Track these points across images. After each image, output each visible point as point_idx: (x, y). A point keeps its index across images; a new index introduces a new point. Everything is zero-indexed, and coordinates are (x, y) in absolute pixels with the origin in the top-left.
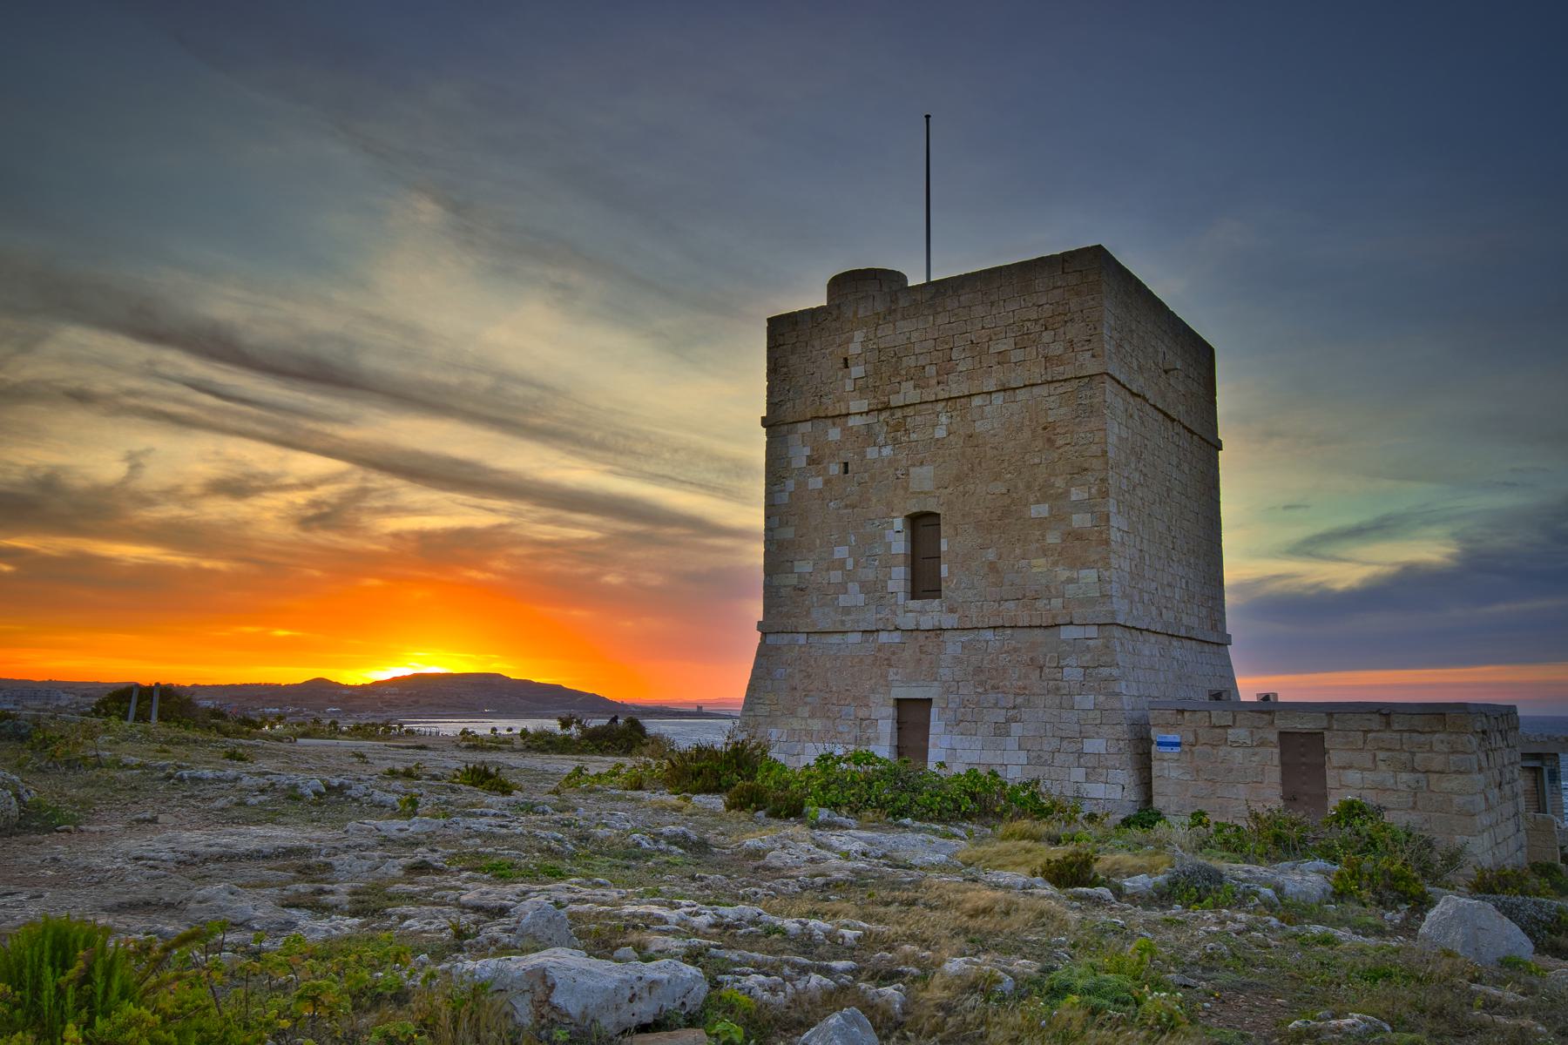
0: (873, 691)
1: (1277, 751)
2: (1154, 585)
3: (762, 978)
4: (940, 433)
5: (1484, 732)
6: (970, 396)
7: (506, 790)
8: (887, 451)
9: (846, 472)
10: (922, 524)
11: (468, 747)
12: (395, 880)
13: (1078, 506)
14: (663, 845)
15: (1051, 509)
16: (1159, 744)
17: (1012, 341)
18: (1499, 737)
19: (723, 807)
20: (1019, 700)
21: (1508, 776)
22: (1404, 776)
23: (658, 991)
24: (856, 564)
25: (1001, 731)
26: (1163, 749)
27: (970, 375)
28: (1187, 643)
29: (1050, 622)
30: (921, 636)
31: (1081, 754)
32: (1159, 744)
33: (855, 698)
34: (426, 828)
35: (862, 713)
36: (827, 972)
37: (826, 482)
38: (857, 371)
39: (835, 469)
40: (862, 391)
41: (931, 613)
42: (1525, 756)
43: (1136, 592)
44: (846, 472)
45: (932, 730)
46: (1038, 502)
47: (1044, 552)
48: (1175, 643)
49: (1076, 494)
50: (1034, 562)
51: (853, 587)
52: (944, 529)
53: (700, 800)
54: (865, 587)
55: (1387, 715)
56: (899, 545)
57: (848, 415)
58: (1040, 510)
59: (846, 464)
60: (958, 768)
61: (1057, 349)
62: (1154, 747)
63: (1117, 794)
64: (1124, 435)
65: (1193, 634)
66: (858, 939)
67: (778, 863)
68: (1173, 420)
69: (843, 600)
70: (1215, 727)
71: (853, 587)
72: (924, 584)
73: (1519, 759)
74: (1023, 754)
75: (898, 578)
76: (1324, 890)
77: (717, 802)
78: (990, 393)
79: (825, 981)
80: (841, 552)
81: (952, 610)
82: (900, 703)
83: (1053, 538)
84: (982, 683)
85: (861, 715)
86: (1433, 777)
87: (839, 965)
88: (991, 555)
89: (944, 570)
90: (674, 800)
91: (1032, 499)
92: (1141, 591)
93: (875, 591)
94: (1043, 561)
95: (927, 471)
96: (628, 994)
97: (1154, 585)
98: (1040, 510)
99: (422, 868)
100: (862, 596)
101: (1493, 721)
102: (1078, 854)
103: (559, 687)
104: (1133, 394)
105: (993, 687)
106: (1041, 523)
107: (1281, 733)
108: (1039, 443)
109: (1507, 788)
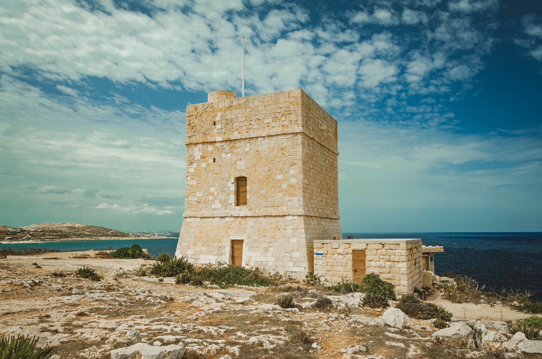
0: (223, 237)
1: (351, 256)
2: (316, 201)
3: (199, 347)
4: (247, 149)
5: (411, 249)
6: (257, 137)
7: (97, 278)
8: (229, 155)
9: (214, 162)
10: (241, 181)
11: (73, 257)
12: (74, 320)
13: (292, 176)
14: (159, 300)
15: (283, 176)
16: (316, 254)
17: (271, 119)
18: (415, 249)
19: (174, 283)
20: (272, 240)
21: (417, 261)
22: (388, 263)
23: (171, 354)
24: (218, 194)
25: (266, 250)
26: (317, 256)
27: (258, 129)
28: (326, 220)
29: (283, 215)
30: (240, 219)
31: (292, 257)
32: (316, 254)
33: (217, 240)
34: (77, 299)
35: (220, 245)
36: (217, 344)
37: (207, 165)
38: (218, 126)
39: (211, 161)
40: (219, 133)
41: (243, 210)
42: (423, 253)
43: (310, 204)
44: (214, 162)
45: (244, 250)
46: (279, 174)
47: (281, 191)
48: (322, 220)
49: (292, 172)
50: (278, 194)
51: (217, 201)
52: (248, 182)
53: (167, 280)
54: (221, 202)
55: (383, 245)
56: (233, 188)
57: (215, 142)
58: (280, 177)
59: (215, 159)
60: (252, 264)
61: (286, 123)
62: (315, 255)
63: (302, 270)
64: (307, 152)
65: (328, 216)
66: (225, 332)
67: (197, 305)
68: (323, 146)
69: (213, 206)
71: (217, 201)
72: (240, 199)
73: (421, 255)
74: (273, 258)
75: (232, 198)
76: (360, 303)
77: (172, 280)
78: (264, 137)
79: (217, 346)
80: (212, 189)
81: (251, 210)
82: (233, 241)
83: (284, 186)
84: (260, 235)
85: (219, 245)
86: (396, 263)
87: (220, 341)
88: (264, 191)
89: (248, 196)
90: (157, 280)
92: (312, 203)
93: (225, 204)
94: (280, 194)
95: (243, 162)
96: (163, 356)
97: (316, 201)
98: (280, 177)
99: (82, 314)
101: (414, 245)
104: (311, 139)
105: (264, 236)
106: (280, 181)
108: (280, 154)
109: (417, 265)
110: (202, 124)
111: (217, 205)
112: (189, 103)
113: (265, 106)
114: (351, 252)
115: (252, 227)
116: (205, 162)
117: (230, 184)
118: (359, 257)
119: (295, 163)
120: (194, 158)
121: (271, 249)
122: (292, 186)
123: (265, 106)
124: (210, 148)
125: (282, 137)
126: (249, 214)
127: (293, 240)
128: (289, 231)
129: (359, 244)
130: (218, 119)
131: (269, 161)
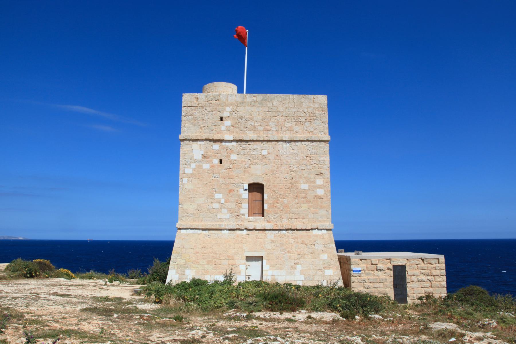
10: (256, 188)
15: (309, 186)
25: (293, 267)
37: (212, 167)
38: (227, 123)
39: (216, 162)
41: (259, 222)
46: (304, 183)
50: (302, 205)
54: (231, 211)
58: (304, 186)
70: (373, 264)
71: (224, 211)
91: (302, 182)
95: (259, 166)
100: (229, 214)
102: (222, 325)
103: (363, 252)
105: (288, 252)
107: (393, 266)
110: (205, 118)
111: (225, 214)
112: (183, 94)
113: (286, 108)
114: (391, 267)
115: (273, 241)
116: (208, 162)
117: (241, 191)
118: (399, 274)
119: (322, 172)
120: (193, 157)
121: (299, 267)
122: (319, 197)
123: (286, 108)
124: (216, 146)
125: (307, 143)
126: (268, 226)
127: (325, 257)
128: (319, 247)
129: (399, 257)
130: (225, 114)
131: (291, 168)
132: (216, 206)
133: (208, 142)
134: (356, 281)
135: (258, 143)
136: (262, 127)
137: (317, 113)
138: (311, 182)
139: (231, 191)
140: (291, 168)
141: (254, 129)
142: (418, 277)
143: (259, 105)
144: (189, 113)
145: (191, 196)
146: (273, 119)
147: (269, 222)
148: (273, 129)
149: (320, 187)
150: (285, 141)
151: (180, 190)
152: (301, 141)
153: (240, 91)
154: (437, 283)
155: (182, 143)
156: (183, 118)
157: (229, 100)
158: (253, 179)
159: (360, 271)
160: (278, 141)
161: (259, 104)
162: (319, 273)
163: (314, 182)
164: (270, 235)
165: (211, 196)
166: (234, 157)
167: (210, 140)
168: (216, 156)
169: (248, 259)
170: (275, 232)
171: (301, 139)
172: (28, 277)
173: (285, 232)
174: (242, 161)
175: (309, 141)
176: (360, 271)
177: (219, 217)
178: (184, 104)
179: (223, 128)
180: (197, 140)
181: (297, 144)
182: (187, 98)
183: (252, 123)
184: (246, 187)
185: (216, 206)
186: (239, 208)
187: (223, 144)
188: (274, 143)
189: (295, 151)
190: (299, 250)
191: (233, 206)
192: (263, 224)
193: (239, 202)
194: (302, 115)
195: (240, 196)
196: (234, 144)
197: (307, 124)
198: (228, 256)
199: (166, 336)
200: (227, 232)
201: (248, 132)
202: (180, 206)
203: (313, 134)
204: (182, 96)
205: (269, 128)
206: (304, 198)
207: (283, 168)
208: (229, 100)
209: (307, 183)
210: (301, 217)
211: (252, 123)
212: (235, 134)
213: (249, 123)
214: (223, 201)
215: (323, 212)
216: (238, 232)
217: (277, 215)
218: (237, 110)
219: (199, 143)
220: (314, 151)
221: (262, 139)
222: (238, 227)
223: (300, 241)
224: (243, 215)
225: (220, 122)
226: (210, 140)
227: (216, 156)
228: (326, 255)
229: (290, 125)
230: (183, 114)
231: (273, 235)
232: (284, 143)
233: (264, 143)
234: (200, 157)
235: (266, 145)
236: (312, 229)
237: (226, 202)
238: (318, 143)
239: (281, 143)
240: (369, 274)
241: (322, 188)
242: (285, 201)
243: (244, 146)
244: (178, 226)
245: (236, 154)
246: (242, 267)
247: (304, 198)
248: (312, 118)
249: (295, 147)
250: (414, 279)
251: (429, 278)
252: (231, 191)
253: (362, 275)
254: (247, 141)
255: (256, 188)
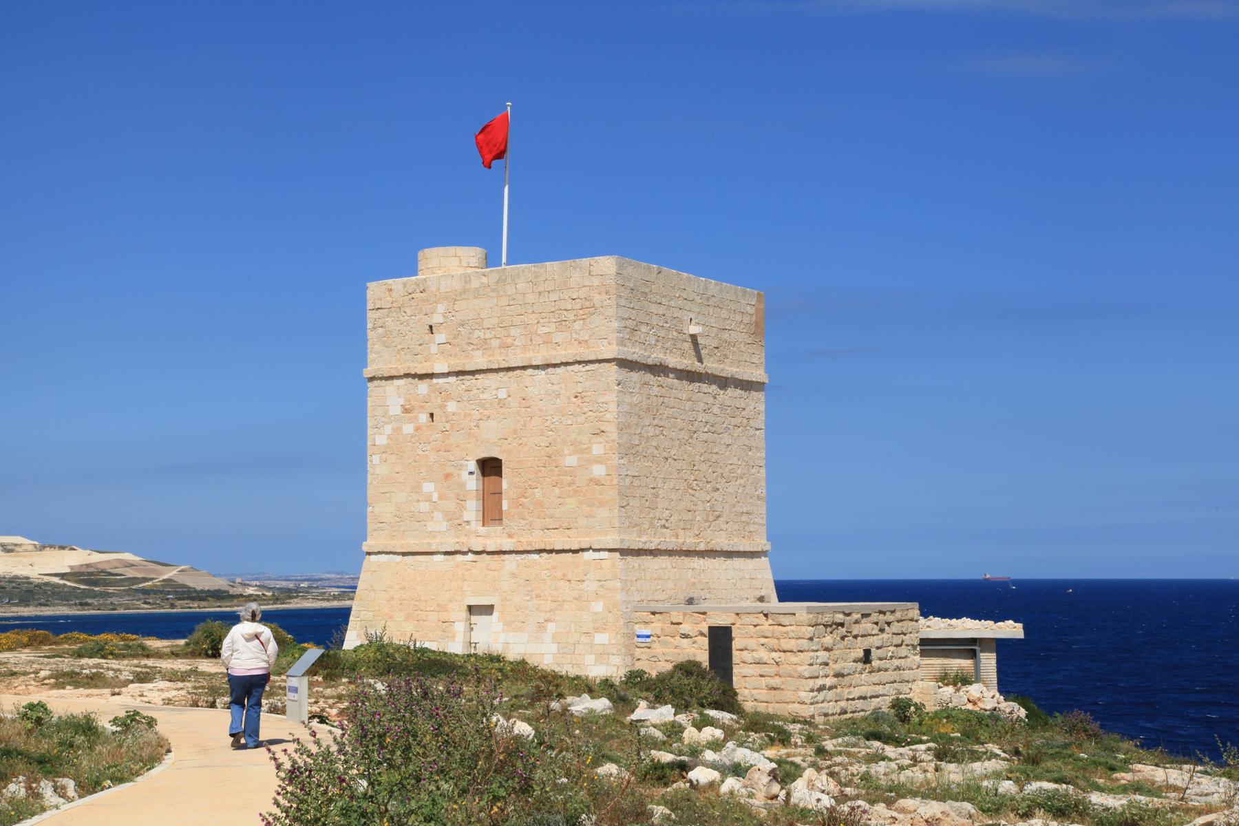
10: (490, 467)
15: (579, 459)
25: (541, 627)
37: (417, 429)
38: (440, 337)
39: (424, 418)
41: (495, 538)
50: (567, 500)
54: (449, 517)
58: (571, 460)
71: (438, 516)
91: (566, 452)
100: (445, 524)
111: (438, 524)
114: (706, 631)
115: (514, 575)
116: (411, 421)
117: (465, 475)
120: (387, 412)
121: (551, 627)
124: (423, 387)
125: (576, 367)
126: (507, 545)
128: (590, 586)
130: (436, 319)
131: (548, 423)
132: (425, 507)
133: (410, 380)
134: (643, 657)
135: (491, 376)
136: (498, 341)
137: (597, 298)
138: (583, 451)
139: (447, 476)
140: (548, 423)
141: (484, 345)
142: (754, 654)
143: (492, 294)
144: (379, 323)
145: (386, 490)
146: (517, 320)
147: (510, 536)
148: (517, 343)
149: (598, 461)
150: (537, 367)
151: (370, 478)
152: (567, 364)
153: (491, 260)
154: (789, 669)
155: (370, 384)
156: (371, 335)
157: (442, 289)
158: (530, 449)
159: (648, 637)
160: (524, 368)
161: (493, 290)
162: (584, 639)
163: (589, 450)
164: (511, 561)
165: (417, 488)
166: (452, 407)
167: (414, 376)
168: (422, 407)
169: (471, 609)
170: (519, 557)
171: (564, 360)
172: (208, 656)
173: (536, 556)
174: (466, 415)
175: (579, 362)
176: (648, 637)
177: (429, 529)
178: (370, 306)
179: (434, 349)
180: (391, 378)
181: (558, 370)
182: (376, 291)
183: (481, 334)
184: (472, 466)
185: (425, 507)
186: (462, 508)
187: (435, 381)
188: (518, 372)
189: (555, 387)
190: (555, 593)
191: (450, 505)
192: (499, 541)
193: (461, 497)
194: (569, 307)
195: (462, 485)
196: (452, 379)
197: (577, 326)
198: (438, 606)
199: (175, 655)
200: (441, 557)
201: (474, 353)
202: (370, 509)
203: (588, 347)
204: (367, 288)
205: (509, 341)
206: (570, 484)
207: (534, 423)
208: (442, 289)
209: (575, 452)
210: (565, 525)
211: (481, 334)
212: (453, 361)
213: (477, 333)
214: (435, 497)
215: (603, 513)
216: (459, 557)
217: (523, 522)
218: (456, 307)
219: (396, 382)
220: (588, 383)
221: (496, 366)
222: (457, 548)
223: (559, 574)
224: (468, 522)
225: (428, 337)
226: (414, 376)
227: (422, 407)
228: (601, 603)
229: (546, 330)
230: (369, 326)
231: (515, 563)
232: (536, 372)
233: (502, 374)
234: (398, 411)
235: (505, 379)
236: (583, 550)
237: (440, 498)
238: (597, 365)
239: (530, 371)
240: (665, 644)
241: (601, 463)
242: (538, 493)
243: (468, 383)
244: (365, 548)
245: (456, 400)
246: (460, 627)
247: (570, 484)
248: (586, 311)
249: (554, 379)
250: (747, 656)
251: (775, 655)
252: (447, 476)
253: (654, 645)
254: (473, 373)
255: (490, 467)
